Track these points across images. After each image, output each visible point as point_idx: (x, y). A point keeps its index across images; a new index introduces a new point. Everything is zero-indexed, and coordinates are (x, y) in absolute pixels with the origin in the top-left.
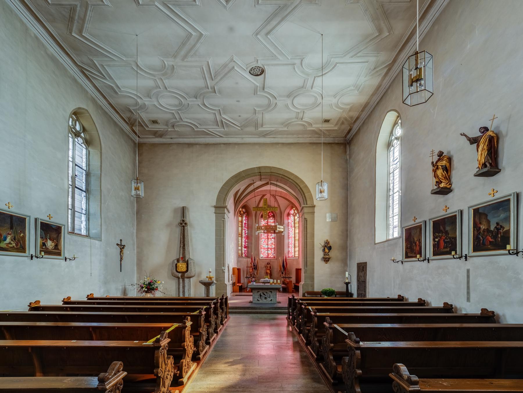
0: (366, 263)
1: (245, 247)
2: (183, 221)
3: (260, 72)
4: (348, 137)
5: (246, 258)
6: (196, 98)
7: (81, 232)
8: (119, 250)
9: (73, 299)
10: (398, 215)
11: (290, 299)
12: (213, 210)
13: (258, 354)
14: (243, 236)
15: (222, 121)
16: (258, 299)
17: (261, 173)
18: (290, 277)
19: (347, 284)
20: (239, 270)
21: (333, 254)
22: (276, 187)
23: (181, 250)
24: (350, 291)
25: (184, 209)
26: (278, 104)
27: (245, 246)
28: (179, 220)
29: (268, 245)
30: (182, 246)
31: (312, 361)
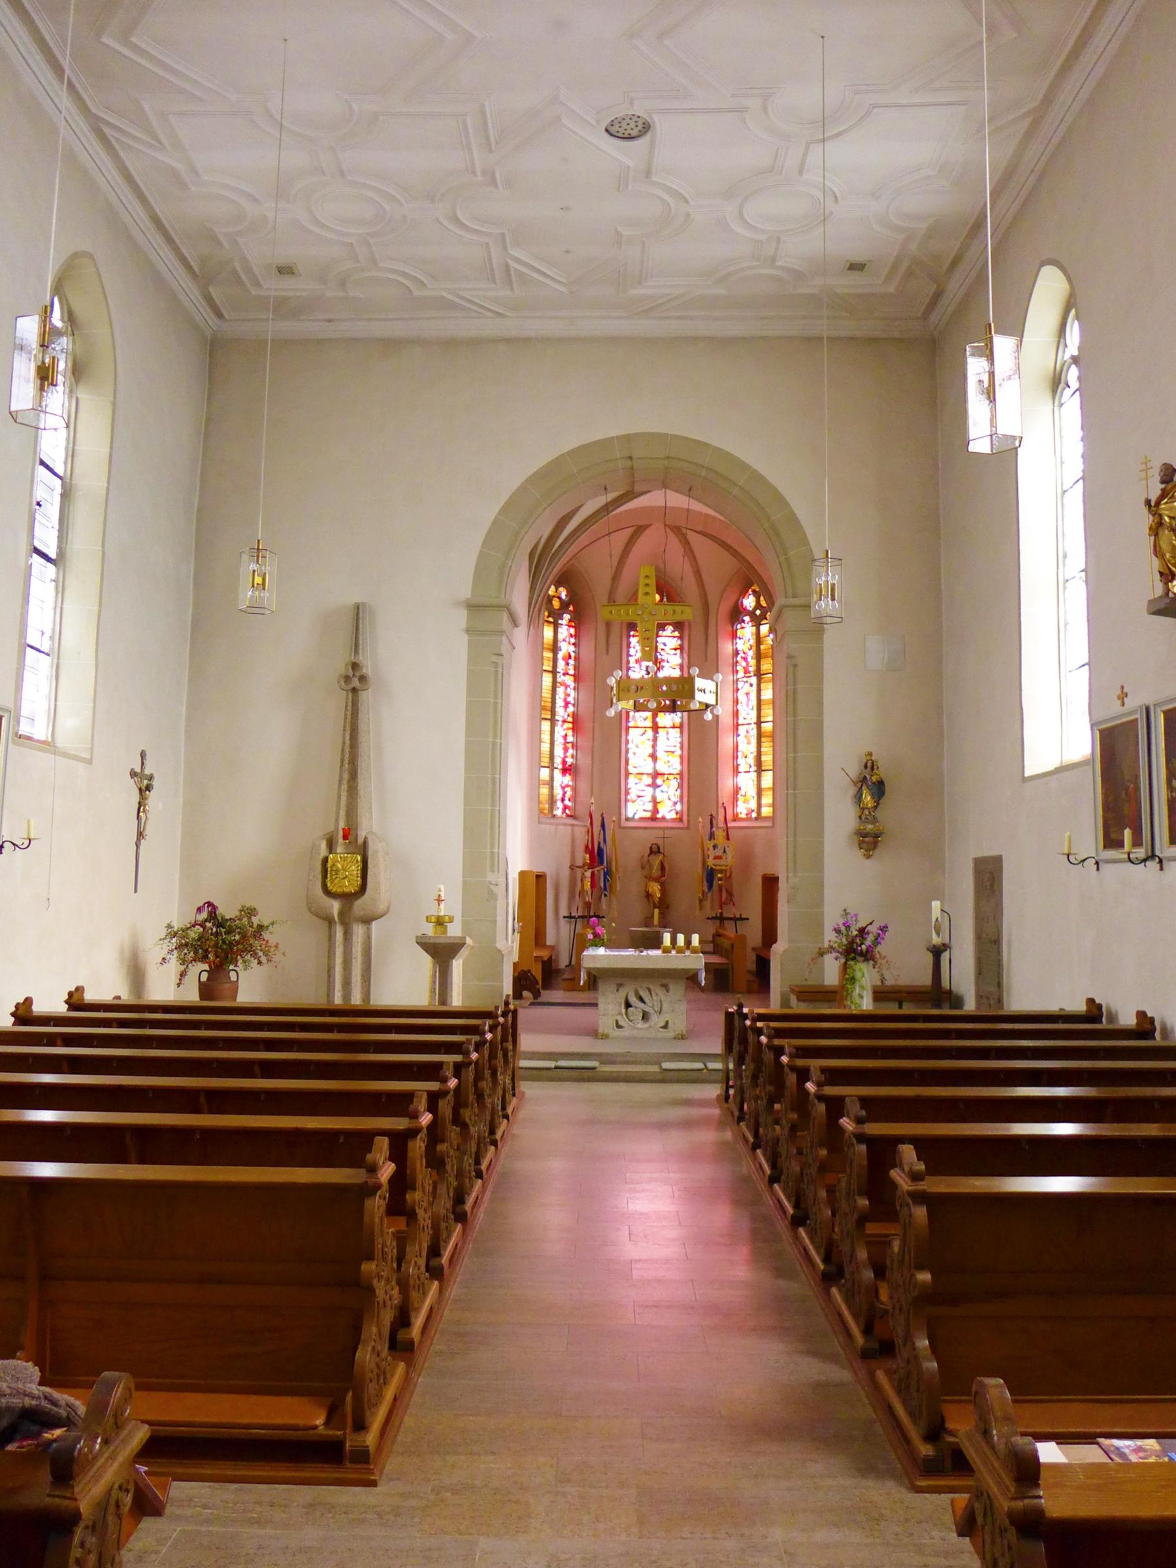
0: (998, 860)
1: (565, 771)
2: (355, 666)
3: (640, 128)
4: (934, 318)
6: (433, 201)
8: (136, 797)
9: (90, 996)
10: (1087, 667)
11: (729, 1016)
12: (461, 617)
13: (626, 1209)
14: (557, 718)
15: (507, 266)
16: (619, 1018)
18: (741, 919)
19: (937, 952)
20: (540, 878)
22: (688, 498)
23: (344, 794)
24: (945, 984)
26: (692, 216)
27: (564, 762)
28: (340, 666)
29: (654, 757)
30: (346, 776)
31: (782, 1227)
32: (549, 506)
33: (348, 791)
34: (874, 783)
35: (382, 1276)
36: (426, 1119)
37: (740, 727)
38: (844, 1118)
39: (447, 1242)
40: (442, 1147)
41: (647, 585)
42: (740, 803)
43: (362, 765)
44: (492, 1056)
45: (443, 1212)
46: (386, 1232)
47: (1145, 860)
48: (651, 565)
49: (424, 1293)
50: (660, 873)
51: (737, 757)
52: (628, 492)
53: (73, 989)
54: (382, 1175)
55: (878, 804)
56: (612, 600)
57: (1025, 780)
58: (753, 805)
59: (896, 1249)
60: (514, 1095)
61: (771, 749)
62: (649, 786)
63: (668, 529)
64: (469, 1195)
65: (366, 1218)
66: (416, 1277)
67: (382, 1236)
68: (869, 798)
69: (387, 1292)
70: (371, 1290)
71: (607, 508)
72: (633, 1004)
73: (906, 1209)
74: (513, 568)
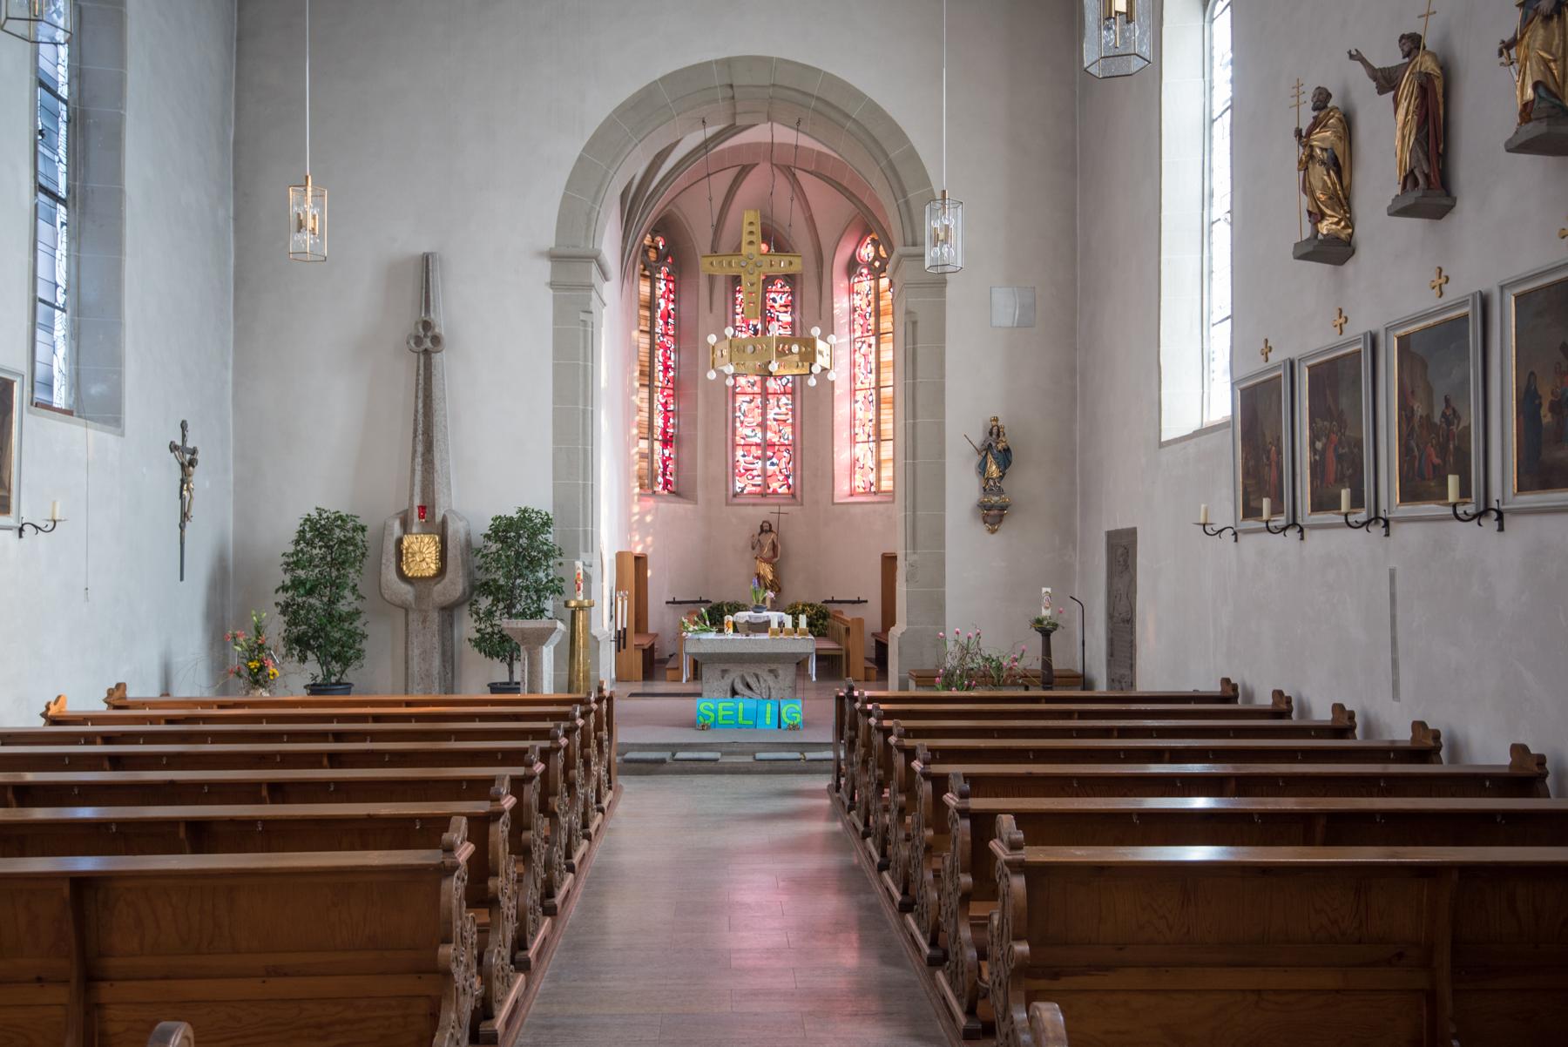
0: (1132, 532)
2: (427, 325)
5: (672, 498)
7: (51, 392)
8: (178, 475)
11: (840, 700)
12: (545, 269)
14: (656, 383)
17: (735, 89)
20: (640, 561)
21: (1026, 482)
22: (795, 132)
23: (418, 468)
25: (430, 268)
27: (664, 432)
28: (407, 323)
29: (763, 426)
30: (420, 449)
31: (890, 914)
32: (640, 141)
33: (423, 465)
34: (1000, 451)
35: (461, 961)
36: (508, 802)
37: (857, 393)
38: (996, 840)
39: (534, 935)
40: (527, 835)
41: (751, 233)
42: (858, 476)
43: (438, 435)
44: (585, 744)
45: (529, 903)
46: (466, 921)
47: (1284, 529)
48: (756, 211)
49: (508, 986)
50: (771, 554)
51: (854, 426)
52: (731, 126)
53: (113, 686)
54: (460, 855)
55: (1004, 474)
56: (714, 250)
57: (1161, 445)
58: (872, 477)
59: (996, 923)
60: (610, 788)
61: (891, 417)
62: (758, 458)
63: (776, 170)
64: (559, 888)
65: (443, 899)
66: (499, 967)
67: (461, 919)
68: (994, 467)
69: (466, 980)
70: (448, 974)
71: (705, 145)
72: (739, 691)
73: (1004, 880)
74: (601, 213)
